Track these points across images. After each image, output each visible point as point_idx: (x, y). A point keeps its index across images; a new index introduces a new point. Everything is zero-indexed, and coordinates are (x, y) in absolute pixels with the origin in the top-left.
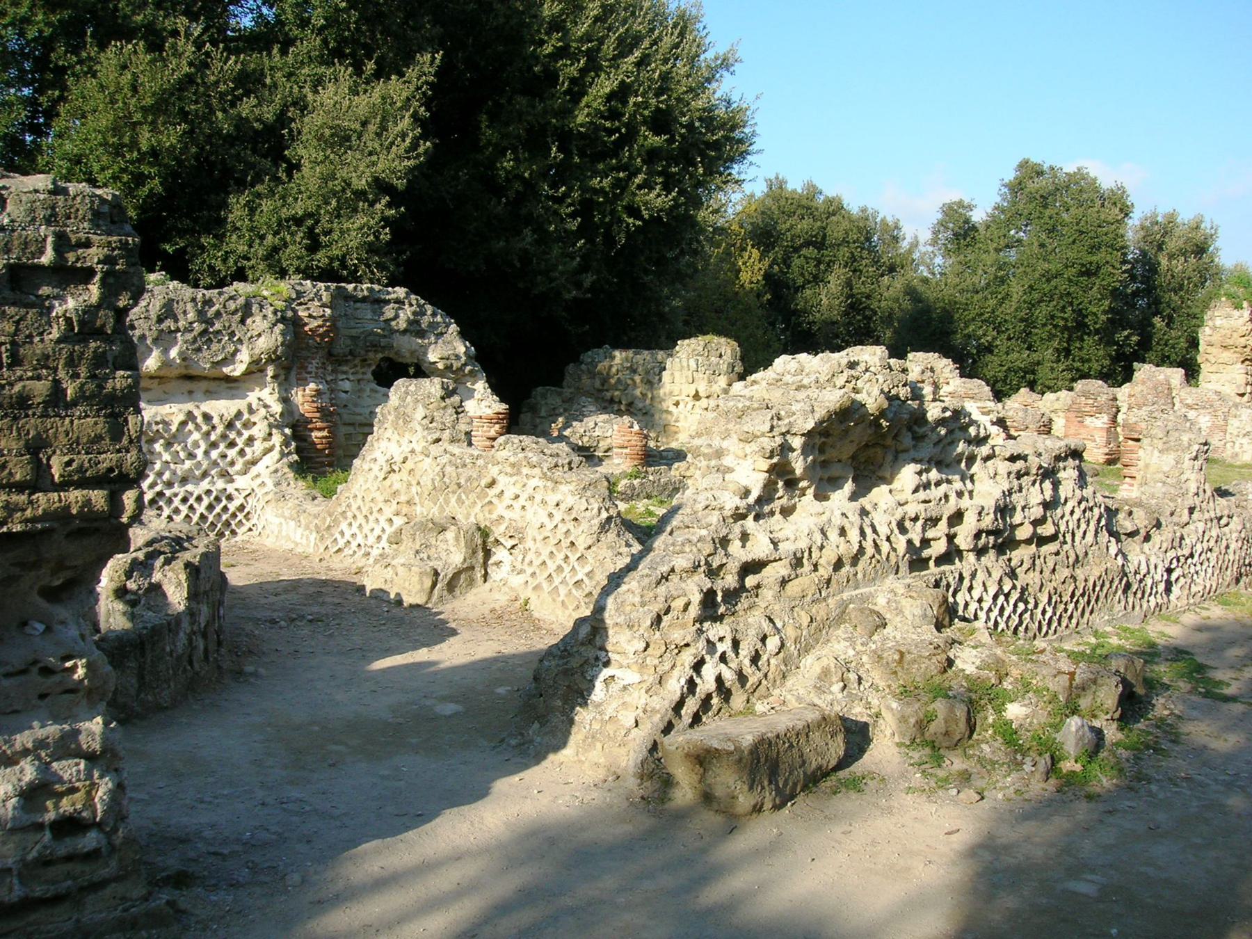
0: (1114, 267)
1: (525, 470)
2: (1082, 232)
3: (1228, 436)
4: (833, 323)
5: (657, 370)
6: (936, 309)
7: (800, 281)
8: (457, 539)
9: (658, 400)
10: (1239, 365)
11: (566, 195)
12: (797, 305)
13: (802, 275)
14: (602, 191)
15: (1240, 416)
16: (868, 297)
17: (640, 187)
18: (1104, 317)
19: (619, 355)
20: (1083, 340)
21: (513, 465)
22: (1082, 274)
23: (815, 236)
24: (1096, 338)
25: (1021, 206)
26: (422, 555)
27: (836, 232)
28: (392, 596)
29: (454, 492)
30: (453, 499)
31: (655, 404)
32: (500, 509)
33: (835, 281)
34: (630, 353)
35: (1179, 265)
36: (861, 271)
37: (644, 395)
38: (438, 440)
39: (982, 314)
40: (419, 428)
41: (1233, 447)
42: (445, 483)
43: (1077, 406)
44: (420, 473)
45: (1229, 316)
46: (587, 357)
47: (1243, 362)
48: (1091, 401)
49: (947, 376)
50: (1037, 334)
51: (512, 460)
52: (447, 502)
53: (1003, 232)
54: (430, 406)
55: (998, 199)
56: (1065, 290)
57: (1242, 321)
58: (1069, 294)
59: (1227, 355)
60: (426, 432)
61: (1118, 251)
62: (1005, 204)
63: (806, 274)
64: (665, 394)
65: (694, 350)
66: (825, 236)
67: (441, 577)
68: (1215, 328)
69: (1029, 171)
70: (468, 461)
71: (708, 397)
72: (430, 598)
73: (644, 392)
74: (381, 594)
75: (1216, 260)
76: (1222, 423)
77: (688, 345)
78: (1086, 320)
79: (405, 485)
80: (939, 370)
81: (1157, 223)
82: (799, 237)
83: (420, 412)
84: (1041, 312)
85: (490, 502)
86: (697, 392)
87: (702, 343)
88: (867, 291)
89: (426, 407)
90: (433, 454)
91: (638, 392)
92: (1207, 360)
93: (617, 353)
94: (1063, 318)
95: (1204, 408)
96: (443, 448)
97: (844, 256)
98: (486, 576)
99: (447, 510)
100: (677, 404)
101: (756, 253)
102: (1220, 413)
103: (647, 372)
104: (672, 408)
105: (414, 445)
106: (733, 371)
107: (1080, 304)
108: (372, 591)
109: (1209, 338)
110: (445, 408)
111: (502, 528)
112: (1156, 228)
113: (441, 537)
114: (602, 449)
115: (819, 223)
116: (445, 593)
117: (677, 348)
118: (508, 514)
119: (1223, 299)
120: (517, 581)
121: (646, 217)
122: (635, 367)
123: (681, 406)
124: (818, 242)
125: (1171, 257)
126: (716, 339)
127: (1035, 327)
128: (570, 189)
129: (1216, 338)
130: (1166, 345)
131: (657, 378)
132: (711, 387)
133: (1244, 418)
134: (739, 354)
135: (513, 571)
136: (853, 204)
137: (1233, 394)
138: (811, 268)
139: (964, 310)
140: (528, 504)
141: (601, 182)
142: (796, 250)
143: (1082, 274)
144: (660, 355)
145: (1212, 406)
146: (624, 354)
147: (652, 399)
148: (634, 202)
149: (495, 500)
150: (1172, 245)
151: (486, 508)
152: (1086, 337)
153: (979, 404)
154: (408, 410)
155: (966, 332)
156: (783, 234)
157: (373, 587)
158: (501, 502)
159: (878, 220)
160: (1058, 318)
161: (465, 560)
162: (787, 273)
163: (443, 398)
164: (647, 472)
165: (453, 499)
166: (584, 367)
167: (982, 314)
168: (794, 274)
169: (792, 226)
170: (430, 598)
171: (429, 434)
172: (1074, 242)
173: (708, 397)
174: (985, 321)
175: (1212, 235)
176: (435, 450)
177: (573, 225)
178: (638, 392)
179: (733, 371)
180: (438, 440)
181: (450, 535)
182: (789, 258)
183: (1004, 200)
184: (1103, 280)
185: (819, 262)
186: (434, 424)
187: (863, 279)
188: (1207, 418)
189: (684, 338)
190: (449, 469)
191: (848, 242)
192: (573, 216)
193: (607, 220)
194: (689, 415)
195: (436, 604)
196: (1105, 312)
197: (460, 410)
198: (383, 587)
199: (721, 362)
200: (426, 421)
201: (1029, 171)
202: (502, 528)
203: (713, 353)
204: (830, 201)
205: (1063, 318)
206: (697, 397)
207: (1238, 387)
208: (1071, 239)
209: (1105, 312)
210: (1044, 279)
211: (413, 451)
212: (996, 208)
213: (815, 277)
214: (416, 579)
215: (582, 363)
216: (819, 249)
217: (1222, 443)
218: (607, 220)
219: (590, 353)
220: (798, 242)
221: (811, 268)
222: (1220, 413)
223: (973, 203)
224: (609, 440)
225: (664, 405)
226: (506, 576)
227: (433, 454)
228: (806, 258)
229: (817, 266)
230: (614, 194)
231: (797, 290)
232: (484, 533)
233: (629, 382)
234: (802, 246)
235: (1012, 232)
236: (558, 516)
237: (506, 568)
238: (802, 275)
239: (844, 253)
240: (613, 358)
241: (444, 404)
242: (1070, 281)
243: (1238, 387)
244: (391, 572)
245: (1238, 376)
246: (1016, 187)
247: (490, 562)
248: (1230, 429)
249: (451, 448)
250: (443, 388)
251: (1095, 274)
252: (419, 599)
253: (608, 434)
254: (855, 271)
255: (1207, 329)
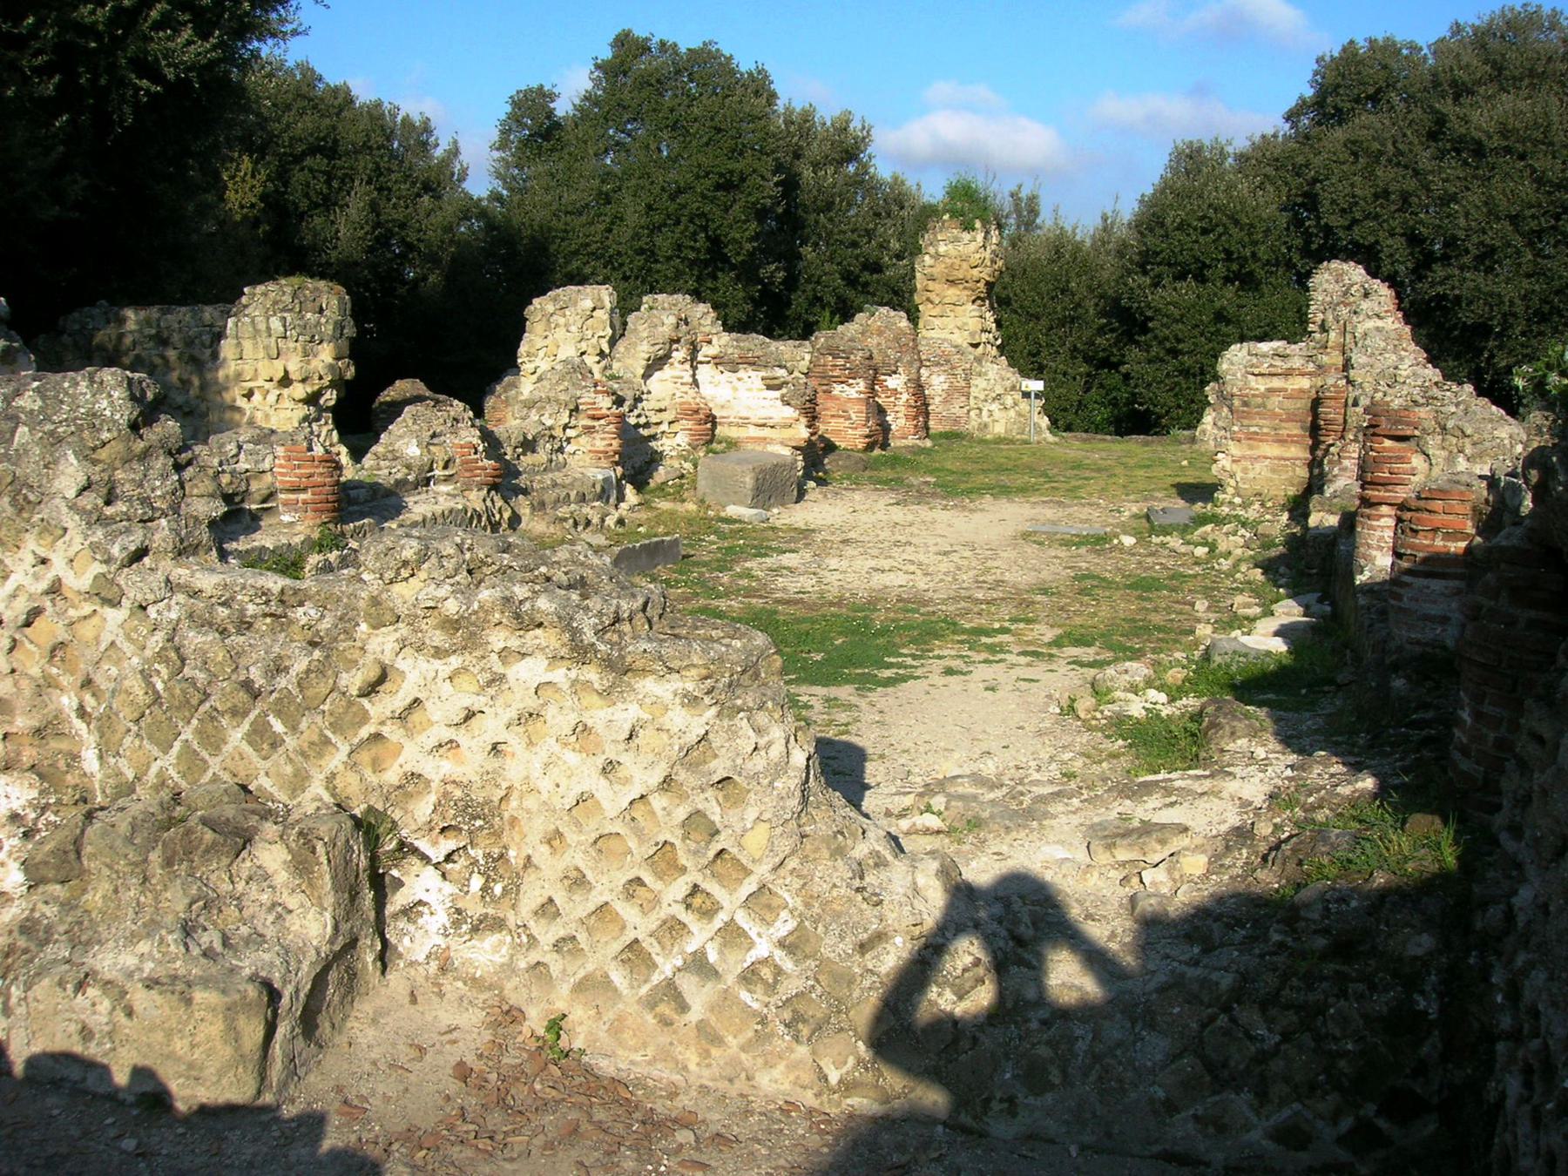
0: (763, 177)
1: (498, 639)
2: (719, 130)
3: (972, 401)
4: (356, 264)
5: (206, 338)
6: (522, 239)
7: (304, 205)
8: (301, 866)
9: (214, 388)
10: (970, 307)
11: (33, 33)
12: (302, 239)
13: (307, 195)
14: (90, 31)
15: (986, 374)
16: (403, 226)
17: (158, 26)
18: (748, 246)
19: (132, 317)
20: (715, 278)
21: (452, 625)
22: (718, 187)
23: (324, 139)
24: (732, 274)
25: (626, 96)
26: (205, 939)
27: (351, 136)
28: (121, 1077)
29: (237, 713)
30: (236, 736)
31: (211, 396)
32: (411, 755)
33: (356, 203)
34: (154, 312)
35: (829, 176)
36: (389, 190)
37: (185, 383)
38: (139, 554)
39: (588, 245)
40: (72, 521)
41: (979, 415)
42: (192, 681)
43: (820, 369)
44: (92, 654)
45: (957, 240)
46: (73, 320)
47: (974, 302)
48: (841, 362)
49: (707, 329)
50: (658, 272)
51: (452, 607)
52: (213, 741)
53: (600, 131)
54: (103, 454)
55: (589, 85)
56: (698, 209)
57: (973, 246)
58: (703, 215)
59: (952, 293)
60: (99, 534)
61: (768, 155)
62: (600, 93)
63: (312, 193)
64: (227, 377)
65: (275, 303)
66: (336, 141)
67: (285, 1001)
68: (937, 256)
69: (628, 46)
70: (251, 609)
71: (303, 381)
72: (262, 1076)
73: (185, 377)
74: (75, 1073)
75: (872, 170)
76: (963, 384)
77: (265, 294)
78: (726, 251)
79: (27, 687)
80: (695, 323)
81: (793, 123)
82: (301, 140)
83: (70, 475)
84: (664, 242)
85: (377, 737)
86: (286, 372)
87: (288, 290)
88: (401, 217)
89: (87, 455)
90: (133, 594)
91: (174, 376)
92: (928, 300)
93: (130, 314)
94: (692, 248)
95: (938, 364)
96: (160, 576)
97: (365, 168)
98: (384, 958)
99: (215, 765)
100: (249, 395)
101: (247, 164)
102: (959, 371)
103: (189, 343)
104: (241, 402)
105: (58, 567)
106: (342, 334)
107: (718, 227)
108: (32, 1062)
109: (930, 270)
110: (145, 456)
111: (423, 808)
112: (792, 129)
113: (245, 866)
114: (257, 497)
115: (327, 121)
116: (300, 1043)
117: (244, 300)
118: (437, 769)
119: (946, 217)
120: (485, 954)
121: (171, 77)
122: (165, 334)
123: (257, 397)
124: (330, 150)
125: (816, 166)
126: (310, 283)
127: (656, 261)
128: (40, 23)
129: (939, 270)
130: (818, 283)
131: (208, 352)
132: (308, 363)
133: (991, 375)
134: (349, 306)
135: (456, 924)
136: (363, 94)
137: (965, 345)
138: (320, 185)
139: (563, 240)
140: (514, 741)
141: (93, 12)
142: (298, 159)
143: (718, 187)
144: (208, 313)
145: (948, 361)
146: (143, 314)
147: (203, 387)
148: (146, 53)
149: (392, 732)
150: (815, 151)
151: (365, 757)
152: (720, 274)
153: (763, 374)
154: (29, 469)
155: (569, 269)
156: (276, 136)
157: (36, 1049)
158: (410, 734)
159: (399, 118)
160: (686, 248)
161: (336, 928)
162: (285, 193)
163: (134, 427)
164: (343, 534)
165: (236, 736)
166: (66, 338)
167: (588, 245)
168: (296, 195)
169: (288, 126)
170: (262, 1076)
171: (112, 537)
172: (707, 144)
173: (303, 381)
174: (593, 254)
175: (864, 138)
176: (135, 585)
177: (50, 87)
178: (174, 376)
179: (342, 334)
180: (139, 554)
181: (272, 856)
182: (287, 171)
183: (596, 86)
184: (750, 194)
185: (330, 177)
186: (120, 507)
187: (394, 200)
188: (942, 378)
189: (254, 282)
190: (194, 639)
191: (370, 148)
192: (45, 71)
193: (103, 82)
194: (272, 412)
195: (284, 1085)
196: (751, 240)
197: (184, 456)
198: (78, 1049)
199: (323, 320)
200: (91, 500)
201: (628, 46)
202: (423, 808)
203: (309, 305)
204: (335, 91)
205: (692, 248)
206: (285, 381)
207: (972, 334)
208: (705, 139)
209: (751, 240)
210: (665, 196)
211: (55, 589)
212: (586, 99)
213: (326, 198)
214: (214, 1029)
215: (62, 332)
216: (330, 158)
217: (965, 410)
218: (103, 82)
219: (76, 315)
220: (299, 149)
221: (320, 185)
222: (959, 371)
223: (556, 91)
224: (268, 478)
225: (227, 397)
226: (440, 940)
227: (133, 594)
228: (311, 170)
229: (328, 182)
230: (114, 38)
231: (301, 216)
232: (368, 828)
233: (158, 361)
234: (304, 154)
235: (611, 132)
236: (642, 775)
237: (436, 920)
238: (307, 195)
239: (365, 163)
240: (122, 321)
241: (140, 446)
242: (704, 197)
243: (972, 334)
244: (105, 1005)
245: (971, 321)
246: (612, 71)
247: (390, 909)
248: (974, 391)
249: (181, 573)
250: (133, 398)
251: (737, 187)
252: (234, 1089)
253: (267, 465)
254: (380, 190)
255: (927, 258)
